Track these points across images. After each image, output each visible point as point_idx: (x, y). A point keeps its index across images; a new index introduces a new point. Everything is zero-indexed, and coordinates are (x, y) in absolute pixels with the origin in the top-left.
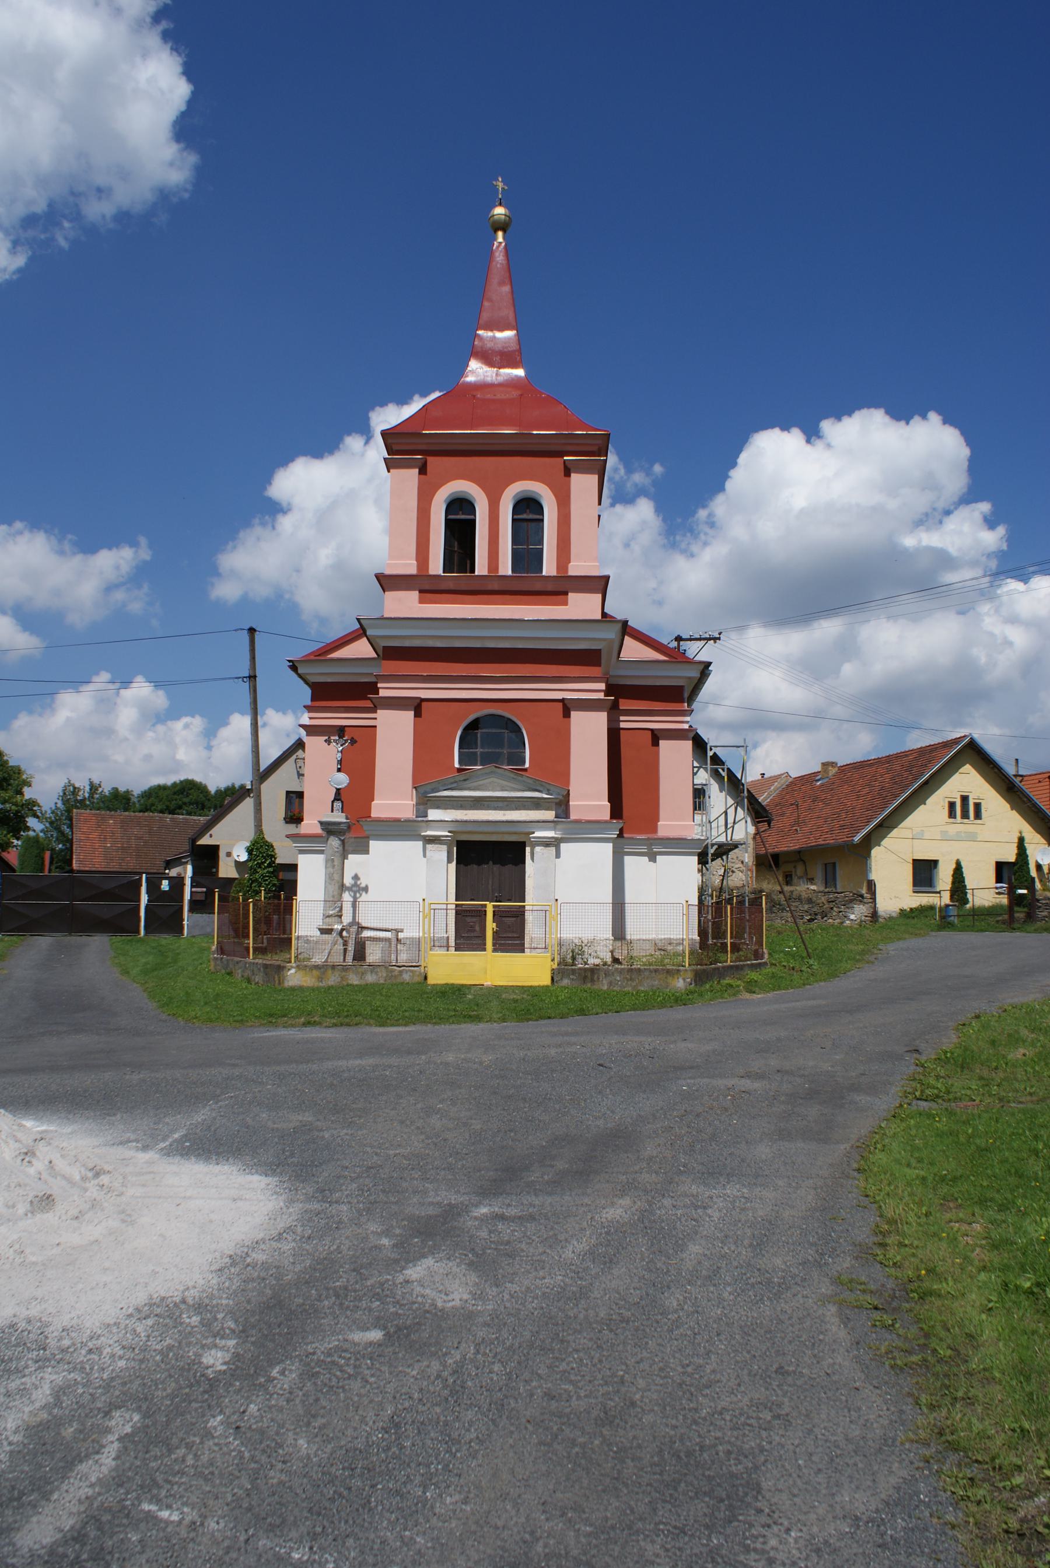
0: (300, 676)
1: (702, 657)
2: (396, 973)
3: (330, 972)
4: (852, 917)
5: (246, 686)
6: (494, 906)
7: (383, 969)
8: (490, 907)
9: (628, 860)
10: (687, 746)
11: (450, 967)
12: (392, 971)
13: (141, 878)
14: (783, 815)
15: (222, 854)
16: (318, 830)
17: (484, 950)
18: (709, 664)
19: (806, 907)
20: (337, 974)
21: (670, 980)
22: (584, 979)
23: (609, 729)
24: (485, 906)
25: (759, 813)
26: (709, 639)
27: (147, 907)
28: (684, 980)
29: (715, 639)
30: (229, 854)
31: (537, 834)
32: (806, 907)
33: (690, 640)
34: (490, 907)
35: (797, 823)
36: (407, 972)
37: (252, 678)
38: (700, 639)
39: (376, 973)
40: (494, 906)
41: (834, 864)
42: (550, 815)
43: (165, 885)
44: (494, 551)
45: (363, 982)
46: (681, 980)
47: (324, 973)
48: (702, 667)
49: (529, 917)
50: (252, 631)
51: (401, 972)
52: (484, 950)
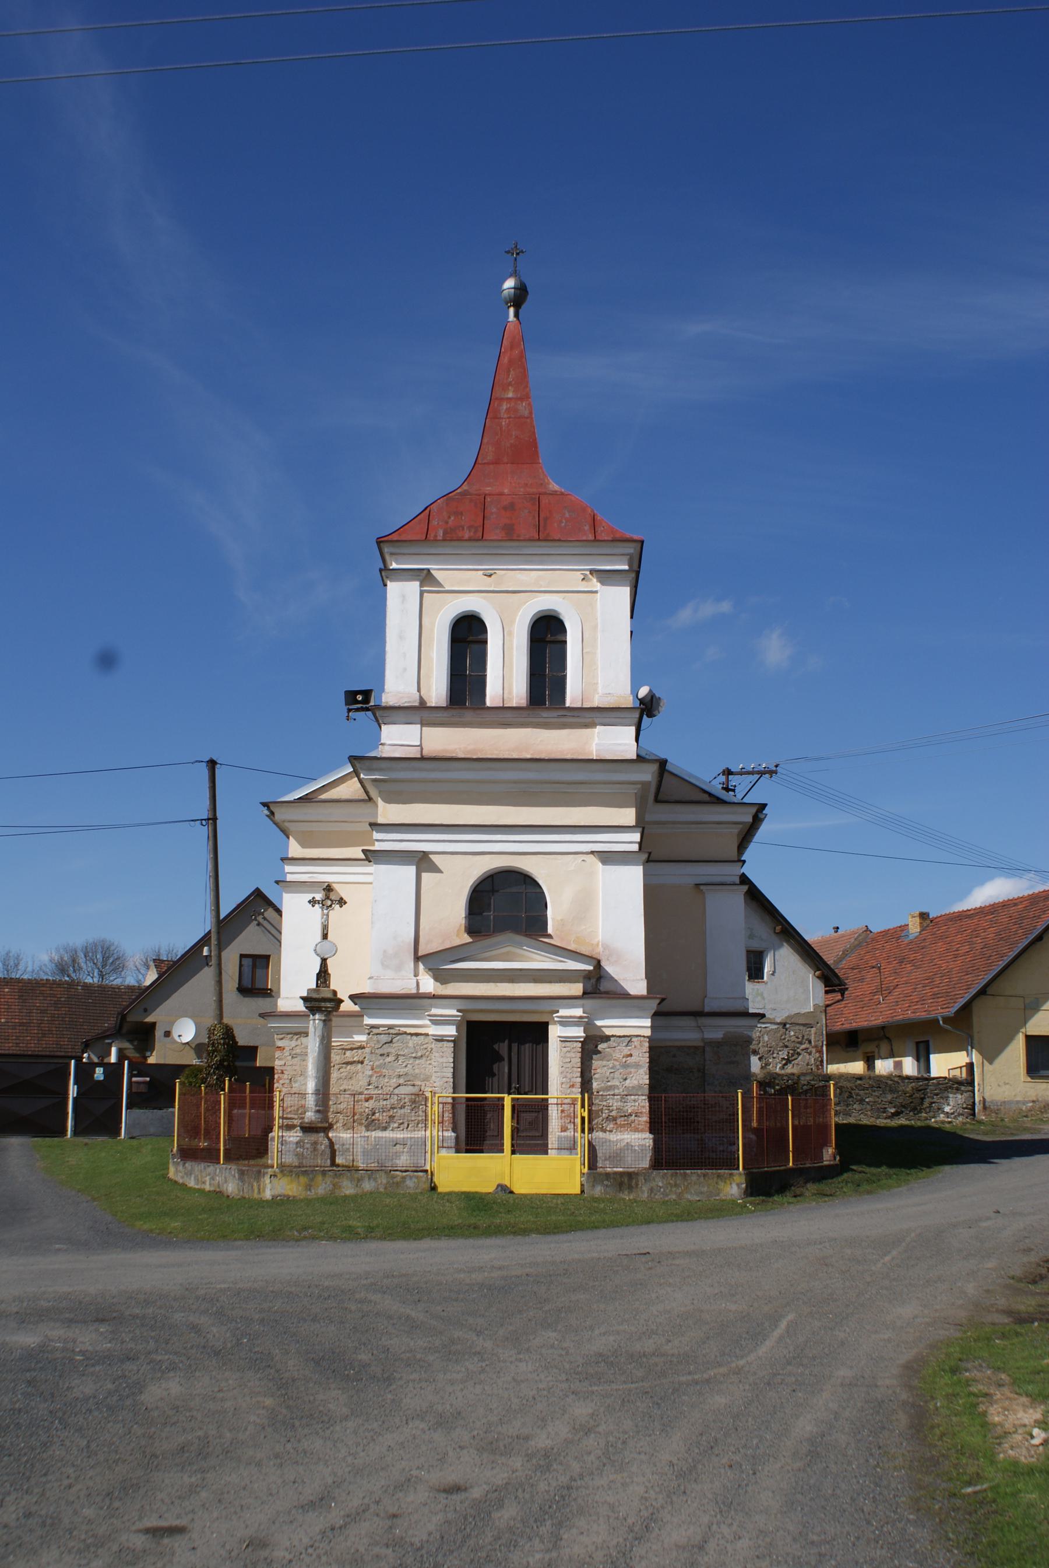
0: (276, 824)
1: (752, 798)
2: (398, 1179)
3: (320, 1178)
4: (947, 1109)
5: (204, 831)
6: (513, 1099)
7: (383, 1174)
8: (508, 1100)
9: (424, 875)
10: (737, 898)
11: (461, 1173)
12: (394, 1177)
13: (69, 1064)
14: (862, 980)
15: (159, 1033)
16: (300, 1007)
17: (502, 1151)
18: (763, 806)
19: (889, 1097)
20: (328, 1180)
21: (721, 1185)
22: (620, 1186)
23: (645, 886)
24: (503, 1098)
25: (831, 980)
26: (761, 773)
27: (74, 1099)
28: (738, 1185)
29: (772, 773)
30: (168, 1034)
31: (563, 1012)
32: (889, 1097)
33: (741, 773)
34: (508, 1100)
35: (880, 990)
36: (411, 1178)
37: (214, 819)
38: (751, 773)
39: (375, 1180)
40: (513, 1099)
41: (927, 1042)
42: (577, 989)
43: (99, 1073)
44: (506, 674)
45: (360, 1191)
46: (735, 1187)
47: (312, 1180)
48: (754, 810)
49: (553, 1113)
50: (212, 764)
51: (404, 1178)
52: (502, 1151)
